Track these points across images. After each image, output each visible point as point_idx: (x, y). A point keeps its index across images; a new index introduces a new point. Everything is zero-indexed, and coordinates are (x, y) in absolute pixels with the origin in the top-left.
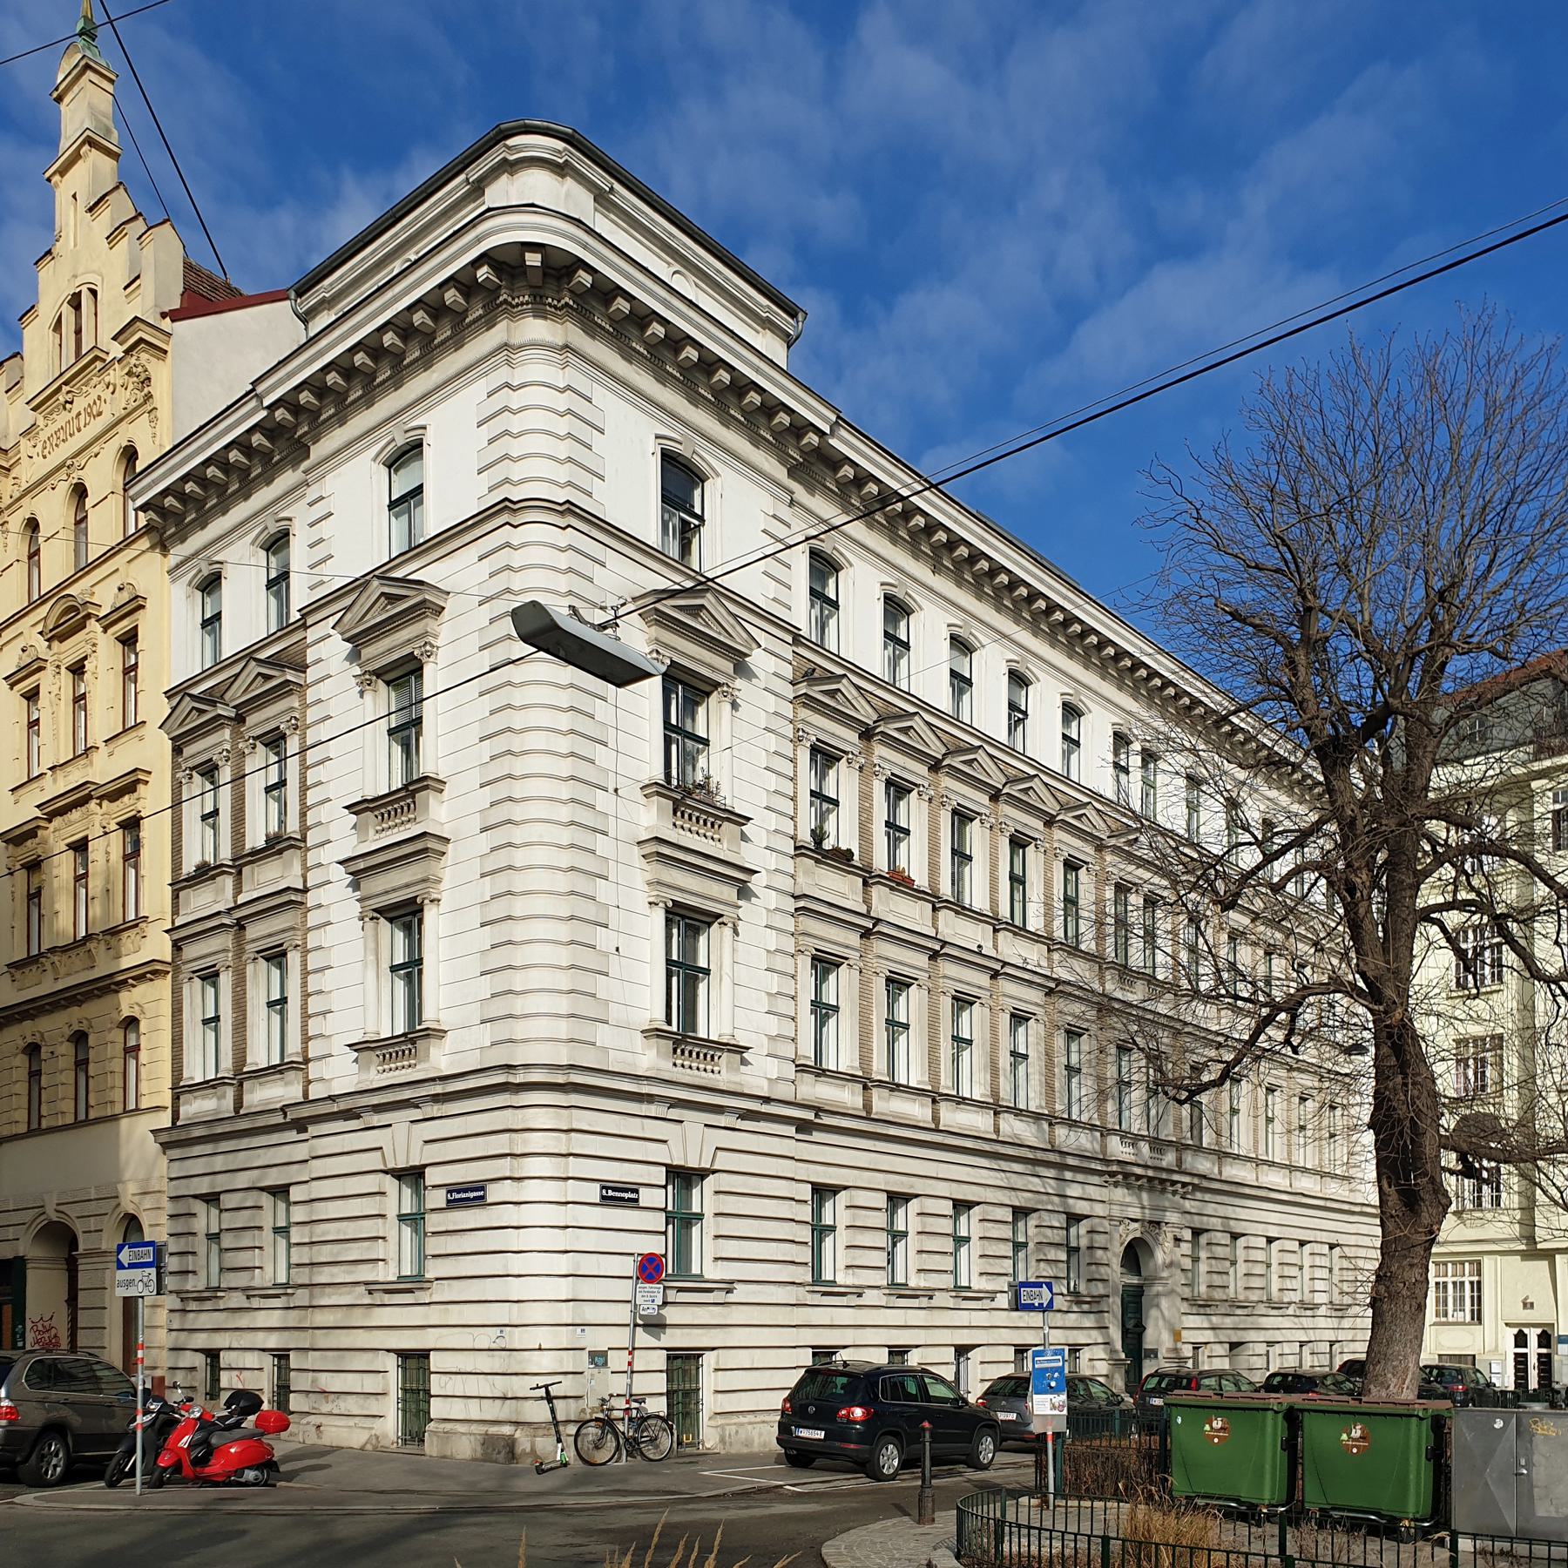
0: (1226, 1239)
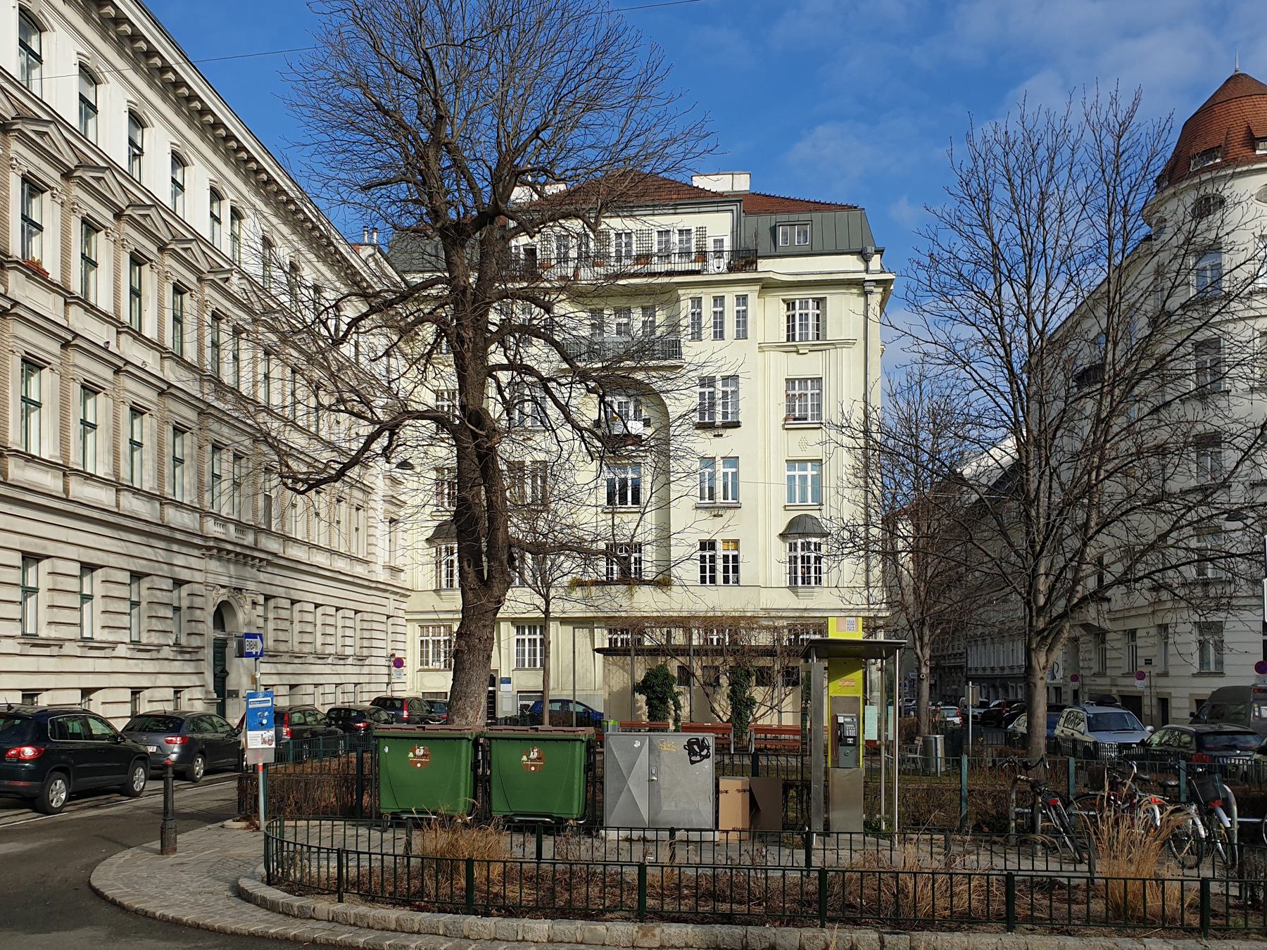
0: (287, 604)
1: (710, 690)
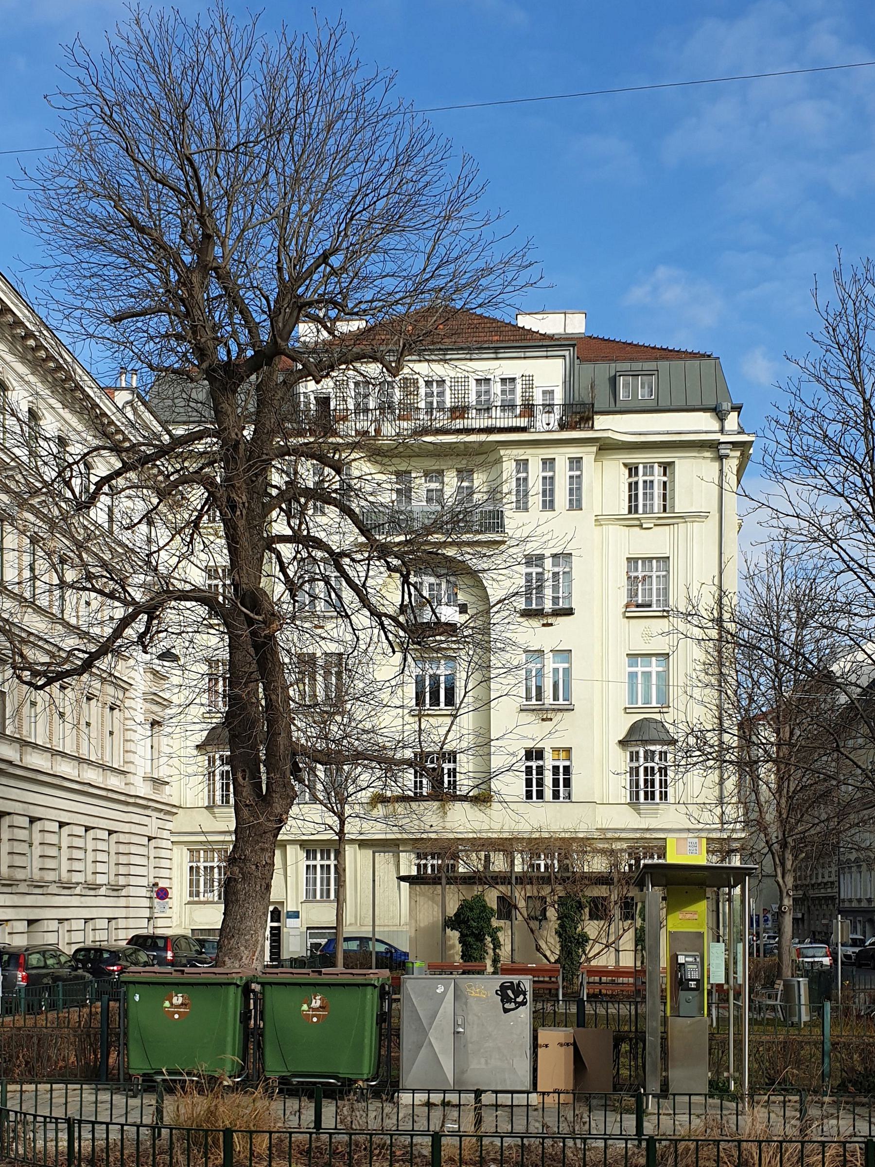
1: (534, 924)
